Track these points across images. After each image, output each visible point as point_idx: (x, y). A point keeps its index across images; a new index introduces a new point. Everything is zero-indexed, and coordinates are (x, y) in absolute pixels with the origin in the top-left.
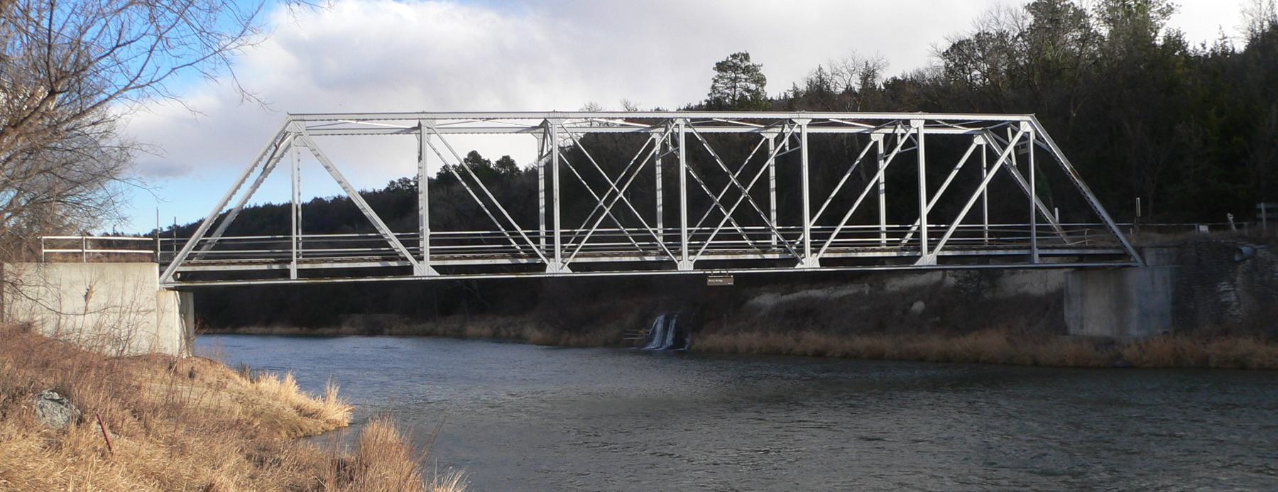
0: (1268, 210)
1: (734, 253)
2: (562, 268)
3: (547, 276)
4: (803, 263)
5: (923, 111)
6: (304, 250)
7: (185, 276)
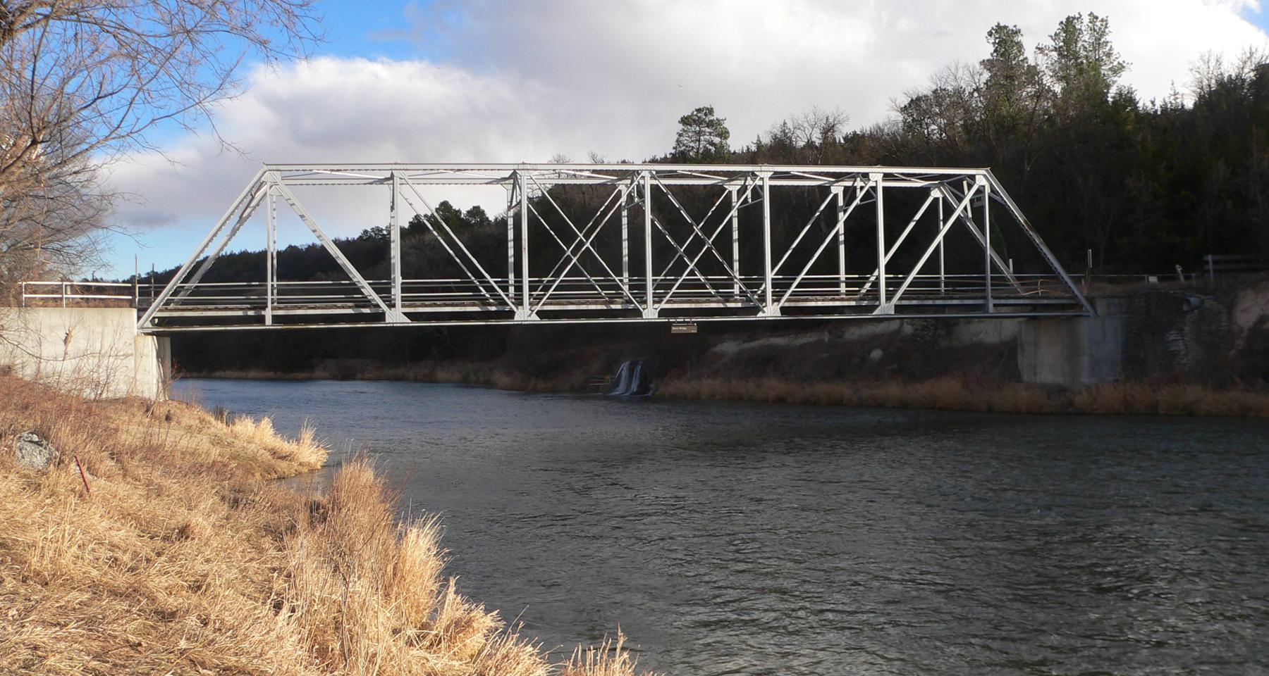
0: (1215, 262)
2: (530, 315)
4: (764, 312)
7: (163, 322)
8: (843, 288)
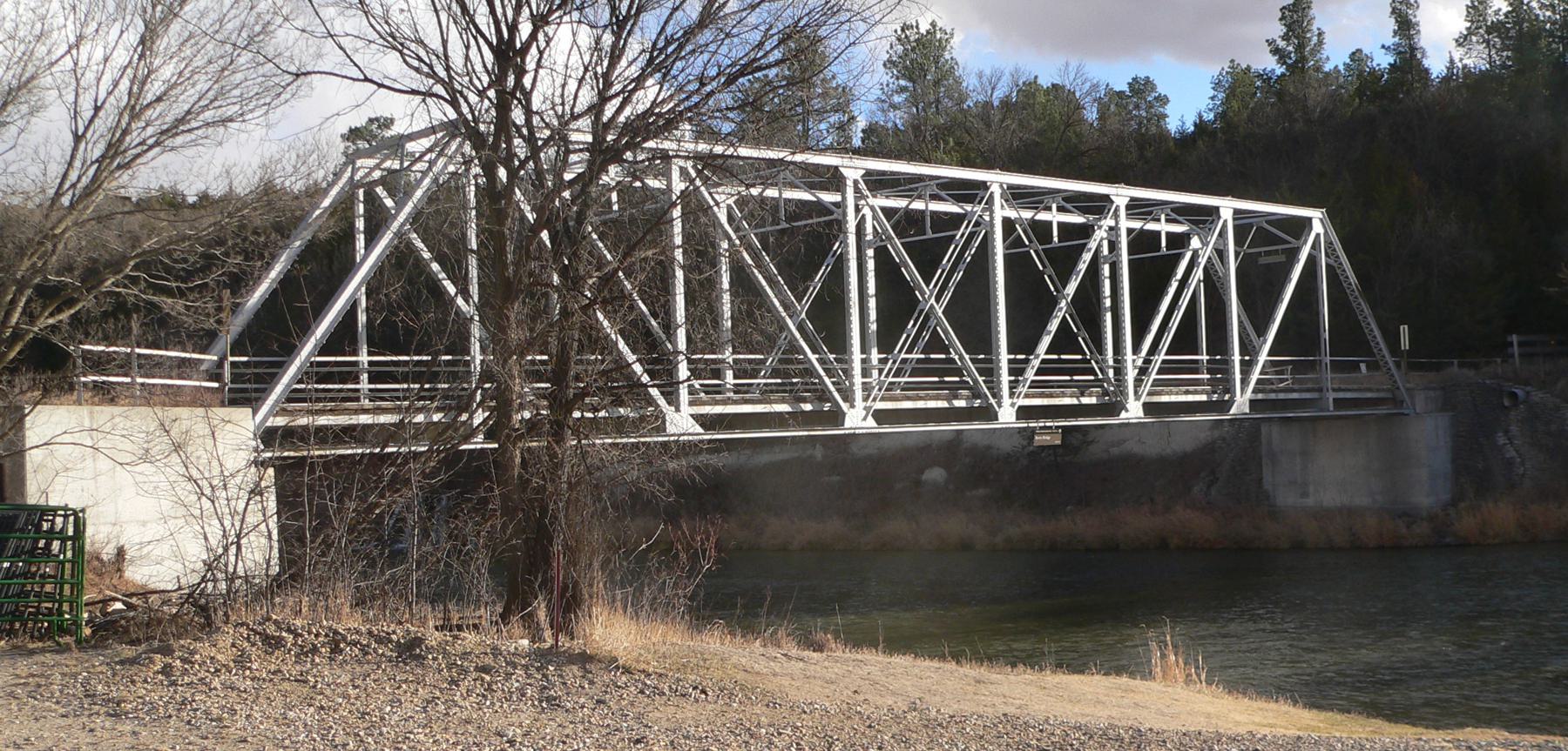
0: (1520, 344)
1: (1051, 396)
2: (865, 419)
3: (847, 432)
4: (1127, 411)
5: (1233, 197)
6: (372, 386)
7: (289, 435)
8: (364, 385)
